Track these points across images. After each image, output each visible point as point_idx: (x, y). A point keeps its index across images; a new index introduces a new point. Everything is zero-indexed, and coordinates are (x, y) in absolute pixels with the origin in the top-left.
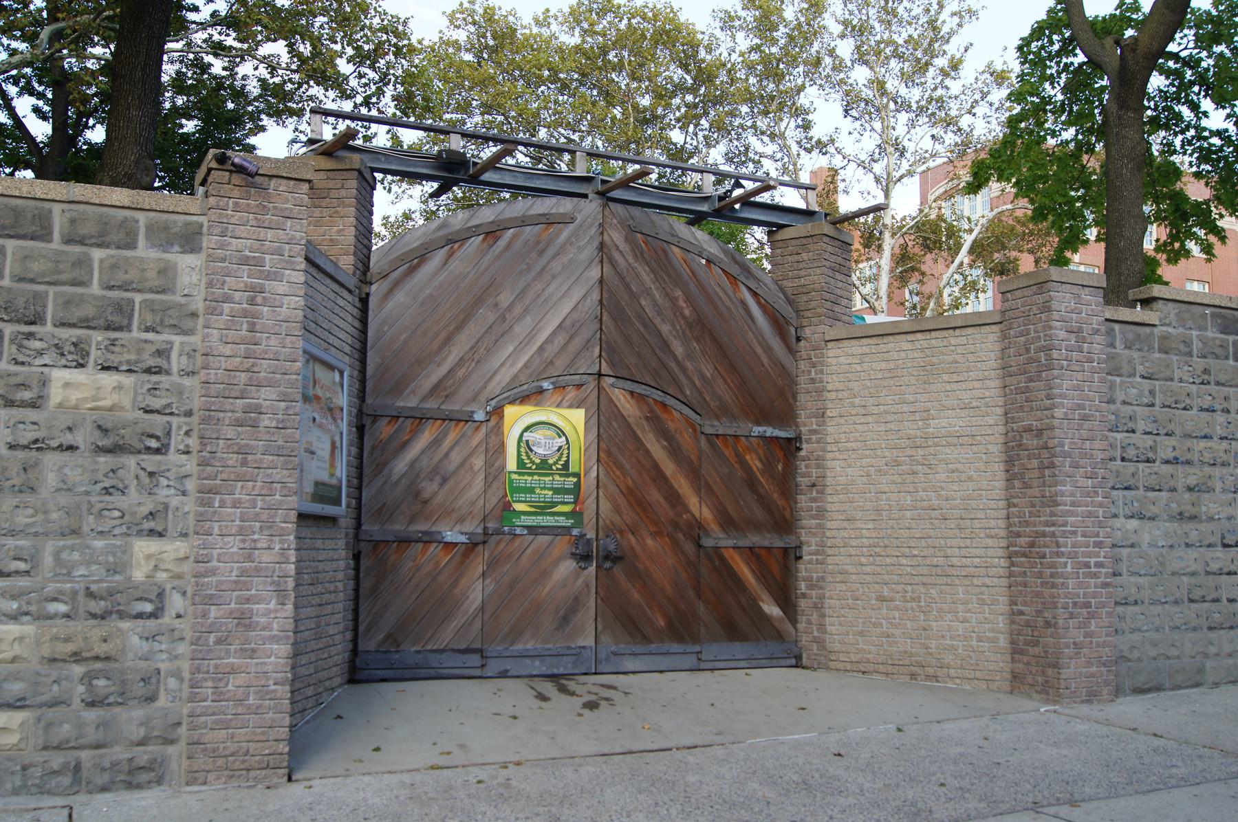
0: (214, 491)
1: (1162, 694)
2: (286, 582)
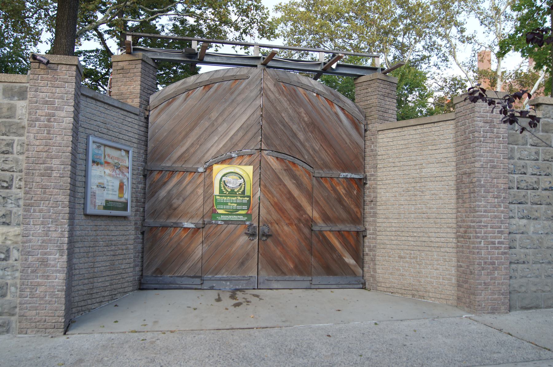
0: (30, 205)
1: (538, 310)
2: (63, 246)
